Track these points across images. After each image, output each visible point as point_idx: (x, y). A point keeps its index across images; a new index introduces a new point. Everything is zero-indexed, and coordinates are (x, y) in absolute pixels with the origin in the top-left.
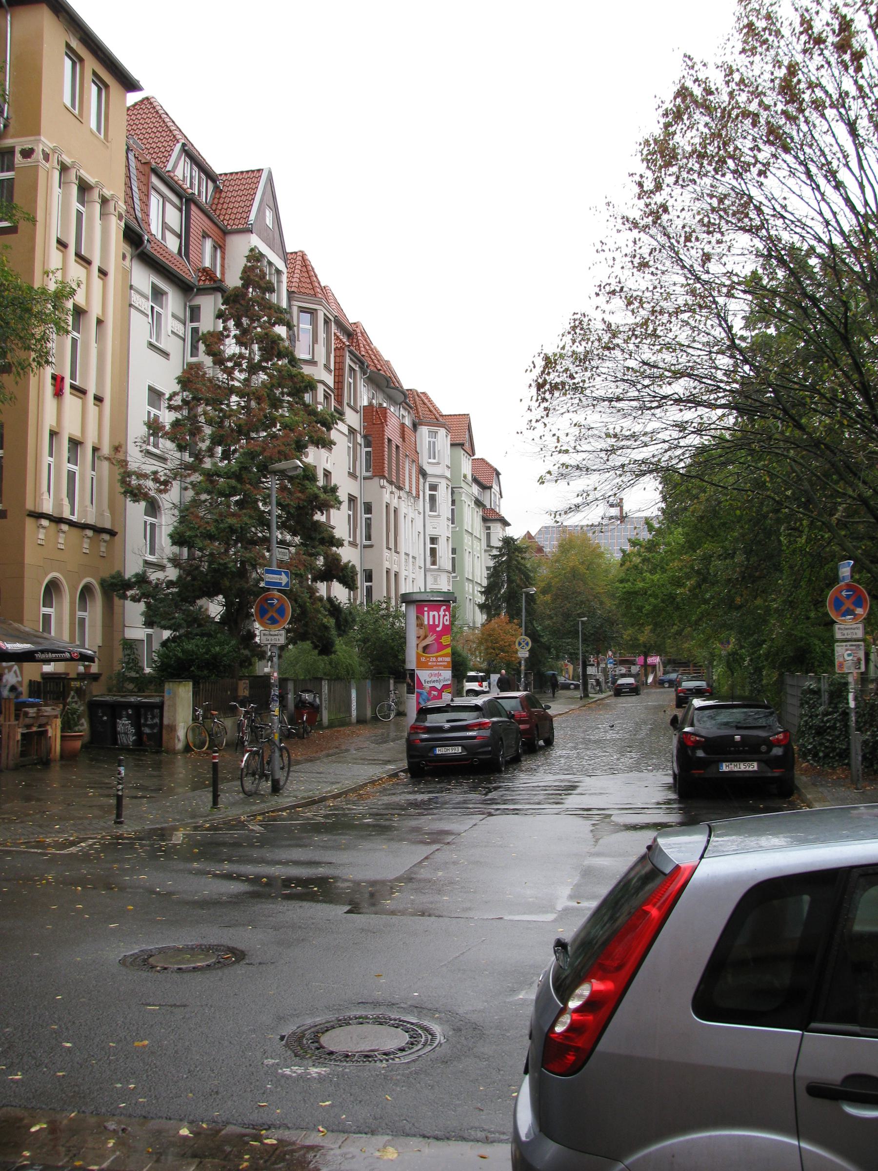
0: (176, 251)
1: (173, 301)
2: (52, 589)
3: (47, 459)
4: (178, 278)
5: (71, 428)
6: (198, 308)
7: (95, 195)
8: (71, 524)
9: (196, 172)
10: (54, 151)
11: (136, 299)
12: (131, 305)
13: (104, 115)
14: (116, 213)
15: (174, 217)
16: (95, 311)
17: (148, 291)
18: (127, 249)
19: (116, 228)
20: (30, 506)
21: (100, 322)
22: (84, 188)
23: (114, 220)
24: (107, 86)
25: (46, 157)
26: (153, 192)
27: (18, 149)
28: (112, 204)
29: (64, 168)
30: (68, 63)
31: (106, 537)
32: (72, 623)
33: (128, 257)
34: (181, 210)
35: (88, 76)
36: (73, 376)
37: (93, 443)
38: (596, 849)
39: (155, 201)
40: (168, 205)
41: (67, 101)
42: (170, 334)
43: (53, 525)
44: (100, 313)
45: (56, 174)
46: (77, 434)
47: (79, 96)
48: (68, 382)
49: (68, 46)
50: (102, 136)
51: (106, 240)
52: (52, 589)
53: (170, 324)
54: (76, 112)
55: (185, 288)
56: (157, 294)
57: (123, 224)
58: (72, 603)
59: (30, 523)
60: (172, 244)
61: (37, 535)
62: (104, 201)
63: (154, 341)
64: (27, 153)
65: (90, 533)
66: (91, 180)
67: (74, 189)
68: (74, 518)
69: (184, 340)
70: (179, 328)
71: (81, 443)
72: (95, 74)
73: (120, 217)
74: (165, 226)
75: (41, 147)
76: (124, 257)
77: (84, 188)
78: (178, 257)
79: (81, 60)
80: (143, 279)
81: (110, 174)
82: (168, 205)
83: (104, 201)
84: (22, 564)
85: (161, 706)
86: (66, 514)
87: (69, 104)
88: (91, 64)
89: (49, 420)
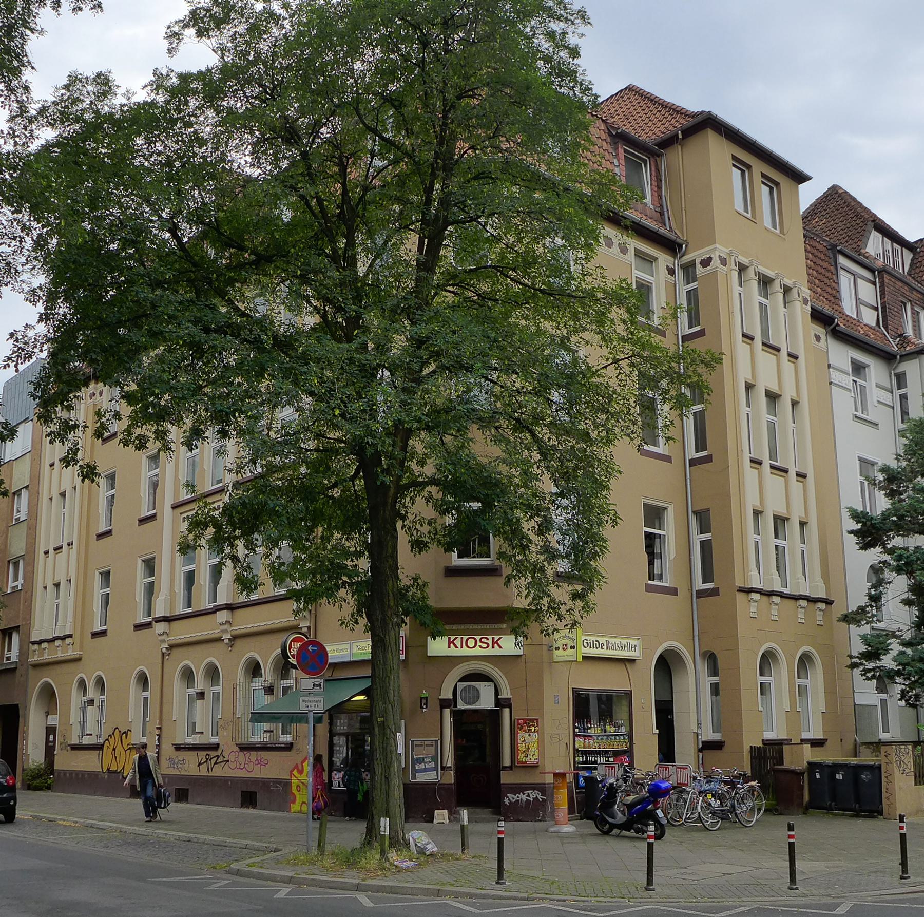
0: (874, 324)
1: (876, 370)
2: (767, 660)
3: (752, 537)
4: (882, 350)
5: (775, 505)
6: (904, 374)
7: (776, 286)
8: (782, 595)
9: (888, 242)
10: (730, 254)
11: (835, 376)
12: (831, 383)
13: (777, 212)
14: (801, 299)
15: (868, 292)
16: (789, 394)
17: (848, 367)
18: (821, 331)
19: (802, 312)
20: (739, 583)
21: (794, 403)
22: (765, 282)
23: (798, 305)
24: (777, 184)
25: (724, 262)
26: (842, 272)
27: (698, 261)
28: (795, 291)
29: (742, 268)
30: (736, 173)
31: (822, 606)
32: (791, 691)
33: (823, 337)
34: (874, 283)
35: (757, 178)
36: (773, 455)
37: (753, 506)
38: (190, 610)
39: (845, 281)
40: (859, 281)
41: (739, 207)
42: (876, 404)
43: (765, 598)
44: (794, 395)
45: (735, 274)
46: (782, 511)
47: (750, 200)
48: (767, 463)
49: (734, 158)
50: (778, 231)
51: (794, 324)
52: (767, 660)
53: (875, 395)
54: (749, 216)
55: (888, 358)
56: (858, 369)
57: (808, 308)
58: (790, 671)
59: (740, 597)
60: (870, 317)
61: (749, 609)
62: (787, 290)
63: (859, 414)
64: (706, 263)
65: (804, 603)
66: (770, 273)
67: (755, 284)
68: (786, 591)
69: (893, 408)
70: (886, 397)
71: (788, 519)
72: (763, 175)
73: (805, 302)
74: (858, 302)
75: (717, 254)
76: (818, 338)
77: (765, 282)
78: (877, 328)
79: (749, 167)
80: (842, 356)
81: (791, 263)
82: (859, 281)
83: (787, 290)
84: (735, 636)
85: (599, 698)
86: (778, 588)
87: (742, 211)
88: (759, 167)
89: (752, 500)
